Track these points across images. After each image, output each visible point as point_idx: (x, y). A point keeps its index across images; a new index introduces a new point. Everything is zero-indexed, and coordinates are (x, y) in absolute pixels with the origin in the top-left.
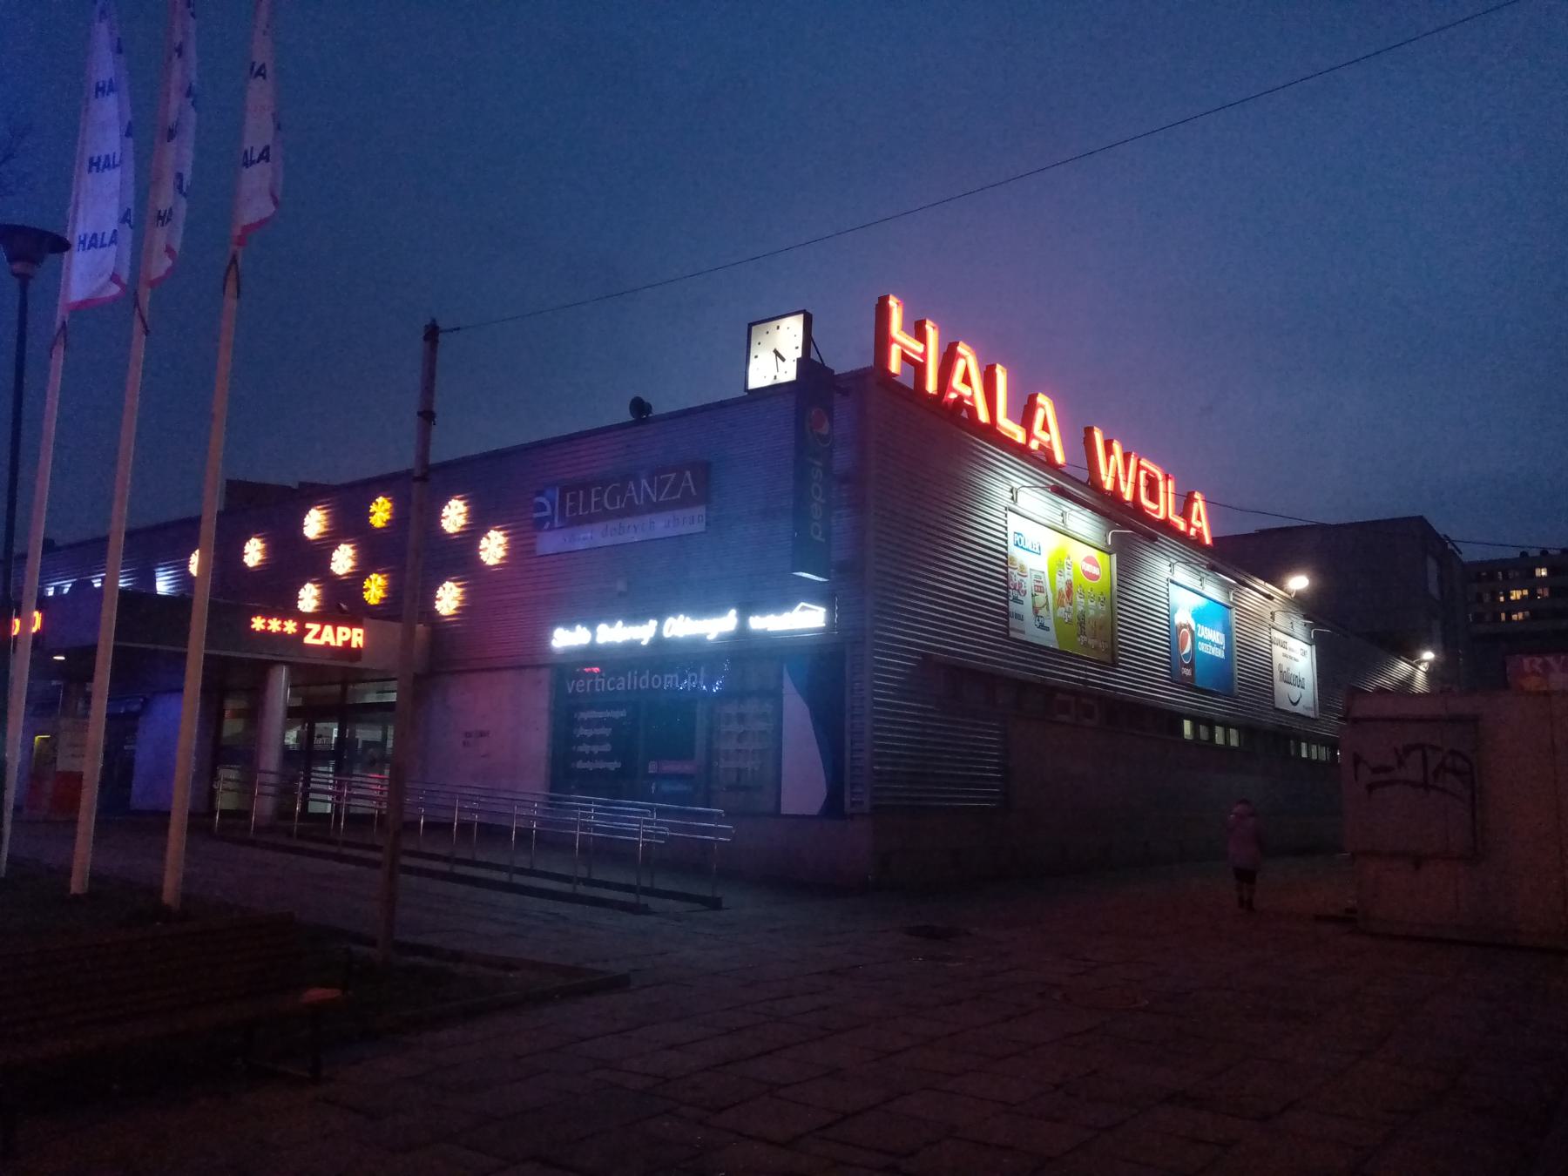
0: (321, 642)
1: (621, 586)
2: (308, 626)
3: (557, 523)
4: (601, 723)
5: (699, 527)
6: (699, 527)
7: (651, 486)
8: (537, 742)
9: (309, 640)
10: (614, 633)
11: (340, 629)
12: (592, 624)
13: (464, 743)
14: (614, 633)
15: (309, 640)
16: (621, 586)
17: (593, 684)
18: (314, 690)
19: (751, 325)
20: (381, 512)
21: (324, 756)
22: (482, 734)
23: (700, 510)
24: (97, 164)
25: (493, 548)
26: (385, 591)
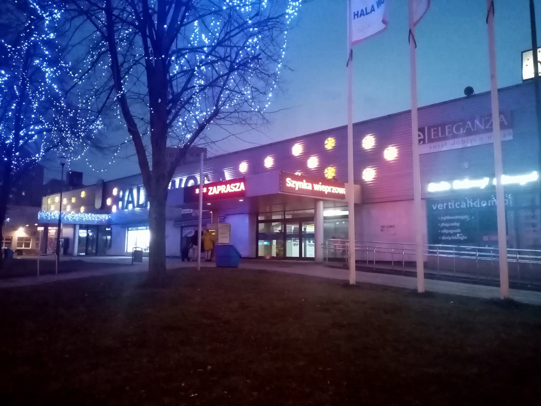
0: (213, 193)
1: (466, 165)
2: (209, 188)
3: (427, 141)
4: (457, 221)
5: (511, 138)
6: (511, 138)
7: (481, 123)
8: (421, 229)
9: (210, 193)
10: (465, 184)
11: (218, 187)
12: (450, 179)
13: (382, 230)
14: (465, 184)
15: (210, 193)
16: (466, 165)
17: (447, 206)
18: (296, 212)
19: (522, 52)
20: (330, 143)
21: (290, 237)
22: (391, 227)
23: (511, 131)
24: (357, 15)
25: (391, 153)
26: (335, 174)
